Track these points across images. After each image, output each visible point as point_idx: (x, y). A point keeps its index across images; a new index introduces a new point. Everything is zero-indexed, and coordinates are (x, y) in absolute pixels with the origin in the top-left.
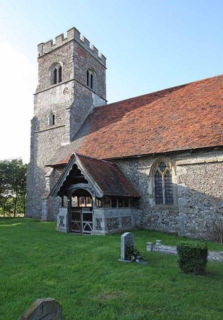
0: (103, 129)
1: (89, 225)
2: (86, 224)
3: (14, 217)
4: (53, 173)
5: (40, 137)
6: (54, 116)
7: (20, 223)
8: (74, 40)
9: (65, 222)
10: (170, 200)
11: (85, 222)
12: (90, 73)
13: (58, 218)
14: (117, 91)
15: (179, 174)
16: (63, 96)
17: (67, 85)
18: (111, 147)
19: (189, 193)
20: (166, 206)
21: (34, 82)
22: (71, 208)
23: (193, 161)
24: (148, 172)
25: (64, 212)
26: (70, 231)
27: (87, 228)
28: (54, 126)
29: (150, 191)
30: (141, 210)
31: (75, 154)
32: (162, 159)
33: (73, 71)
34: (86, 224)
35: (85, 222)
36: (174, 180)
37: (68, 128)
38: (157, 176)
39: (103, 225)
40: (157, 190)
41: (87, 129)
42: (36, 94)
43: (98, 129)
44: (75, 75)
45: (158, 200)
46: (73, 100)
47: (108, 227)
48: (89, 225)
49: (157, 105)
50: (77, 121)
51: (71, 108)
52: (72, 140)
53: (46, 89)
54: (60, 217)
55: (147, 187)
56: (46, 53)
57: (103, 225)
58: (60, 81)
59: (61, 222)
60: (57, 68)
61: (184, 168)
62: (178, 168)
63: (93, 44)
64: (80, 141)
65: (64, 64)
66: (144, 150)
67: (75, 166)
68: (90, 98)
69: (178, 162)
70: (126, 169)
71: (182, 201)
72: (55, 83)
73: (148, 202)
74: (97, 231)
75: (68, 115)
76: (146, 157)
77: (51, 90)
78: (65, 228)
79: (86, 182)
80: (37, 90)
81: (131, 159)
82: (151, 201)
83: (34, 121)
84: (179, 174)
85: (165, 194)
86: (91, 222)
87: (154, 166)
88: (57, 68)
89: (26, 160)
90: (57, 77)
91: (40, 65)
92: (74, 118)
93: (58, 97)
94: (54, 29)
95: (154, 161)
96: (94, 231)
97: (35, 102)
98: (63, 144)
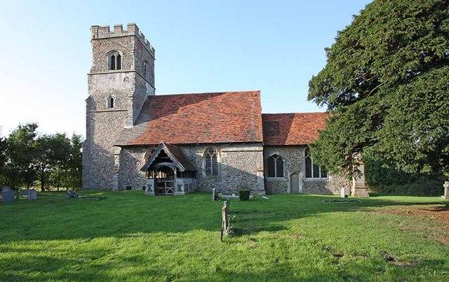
0: (163, 119)
3: (58, 191)
4: (122, 152)
5: (97, 117)
6: (112, 100)
8: (135, 35)
9: (152, 188)
10: (215, 173)
12: (145, 64)
14: (164, 86)
15: (222, 157)
16: (122, 83)
17: (128, 75)
19: (228, 168)
21: (89, 63)
22: (156, 180)
23: (231, 149)
24: (202, 155)
25: (152, 182)
26: (156, 194)
27: (170, 191)
29: (203, 167)
32: (211, 147)
33: (133, 63)
36: (219, 160)
37: (130, 112)
38: (207, 157)
39: (183, 188)
40: (208, 165)
41: (146, 116)
42: (91, 75)
43: (157, 117)
44: (136, 67)
45: (208, 172)
46: (134, 89)
47: (186, 190)
49: (205, 104)
50: (137, 108)
51: (134, 96)
52: (135, 124)
56: (101, 37)
57: (183, 188)
58: (119, 68)
60: (115, 55)
61: (226, 154)
62: (222, 153)
63: (147, 38)
64: (144, 126)
65: (124, 54)
66: (200, 140)
67: (163, 151)
68: (145, 88)
69: (222, 150)
70: (187, 152)
71: (224, 173)
73: (202, 174)
75: (130, 102)
76: (202, 145)
77: (109, 75)
78: (153, 193)
79: (172, 162)
80: (92, 71)
81: (193, 146)
82: (204, 173)
83: (90, 101)
84: (222, 157)
85: (213, 169)
88: (115, 55)
89: (83, 138)
90: (115, 63)
91: (94, 47)
92: (135, 106)
93: (117, 83)
94: (115, 18)
95: (206, 147)
96: (176, 193)
97: (90, 82)
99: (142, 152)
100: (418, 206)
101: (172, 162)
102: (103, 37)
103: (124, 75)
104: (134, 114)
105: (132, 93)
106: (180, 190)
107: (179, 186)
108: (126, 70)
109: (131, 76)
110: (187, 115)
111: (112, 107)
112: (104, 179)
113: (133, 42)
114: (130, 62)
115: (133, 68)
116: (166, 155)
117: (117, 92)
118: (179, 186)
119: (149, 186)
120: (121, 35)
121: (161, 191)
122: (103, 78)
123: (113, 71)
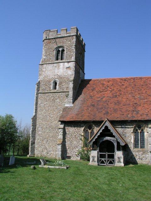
1: (112, 161)
2: (101, 161)
6: (56, 84)
7: (29, 163)
9: (96, 159)
11: (101, 159)
13: (91, 157)
18: (108, 113)
20: (141, 149)
28: (55, 91)
29: (132, 141)
30: (127, 152)
31: (107, 120)
34: (101, 161)
35: (101, 159)
44: (76, 58)
48: (112, 161)
53: (50, 63)
54: (93, 157)
55: (131, 139)
59: (93, 160)
60: (60, 49)
66: (129, 117)
67: (106, 127)
72: (57, 59)
74: (118, 164)
75: (71, 85)
76: (131, 122)
77: (55, 65)
79: (114, 137)
86: (105, 159)
87: (135, 127)
88: (60, 49)
95: (136, 123)
98: (66, 105)
99: (80, 127)
100: (59, 91)
101: (114, 137)
102: (53, 37)
103: (66, 65)
104: (74, 93)
105: (72, 78)
106: (119, 162)
107: (119, 158)
108: (68, 61)
109: (72, 65)
110: (116, 96)
111: (55, 89)
112: (46, 148)
113: (74, 40)
114: (71, 53)
115: (73, 59)
116: (110, 130)
117: (60, 77)
118: (119, 158)
119: (93, 157)
120: (66, 35)
121: (103, 162)
122: (50, 67)
123: (56, 61)
